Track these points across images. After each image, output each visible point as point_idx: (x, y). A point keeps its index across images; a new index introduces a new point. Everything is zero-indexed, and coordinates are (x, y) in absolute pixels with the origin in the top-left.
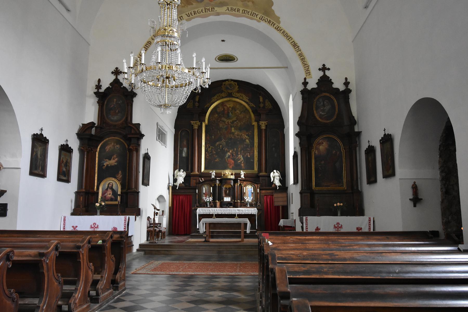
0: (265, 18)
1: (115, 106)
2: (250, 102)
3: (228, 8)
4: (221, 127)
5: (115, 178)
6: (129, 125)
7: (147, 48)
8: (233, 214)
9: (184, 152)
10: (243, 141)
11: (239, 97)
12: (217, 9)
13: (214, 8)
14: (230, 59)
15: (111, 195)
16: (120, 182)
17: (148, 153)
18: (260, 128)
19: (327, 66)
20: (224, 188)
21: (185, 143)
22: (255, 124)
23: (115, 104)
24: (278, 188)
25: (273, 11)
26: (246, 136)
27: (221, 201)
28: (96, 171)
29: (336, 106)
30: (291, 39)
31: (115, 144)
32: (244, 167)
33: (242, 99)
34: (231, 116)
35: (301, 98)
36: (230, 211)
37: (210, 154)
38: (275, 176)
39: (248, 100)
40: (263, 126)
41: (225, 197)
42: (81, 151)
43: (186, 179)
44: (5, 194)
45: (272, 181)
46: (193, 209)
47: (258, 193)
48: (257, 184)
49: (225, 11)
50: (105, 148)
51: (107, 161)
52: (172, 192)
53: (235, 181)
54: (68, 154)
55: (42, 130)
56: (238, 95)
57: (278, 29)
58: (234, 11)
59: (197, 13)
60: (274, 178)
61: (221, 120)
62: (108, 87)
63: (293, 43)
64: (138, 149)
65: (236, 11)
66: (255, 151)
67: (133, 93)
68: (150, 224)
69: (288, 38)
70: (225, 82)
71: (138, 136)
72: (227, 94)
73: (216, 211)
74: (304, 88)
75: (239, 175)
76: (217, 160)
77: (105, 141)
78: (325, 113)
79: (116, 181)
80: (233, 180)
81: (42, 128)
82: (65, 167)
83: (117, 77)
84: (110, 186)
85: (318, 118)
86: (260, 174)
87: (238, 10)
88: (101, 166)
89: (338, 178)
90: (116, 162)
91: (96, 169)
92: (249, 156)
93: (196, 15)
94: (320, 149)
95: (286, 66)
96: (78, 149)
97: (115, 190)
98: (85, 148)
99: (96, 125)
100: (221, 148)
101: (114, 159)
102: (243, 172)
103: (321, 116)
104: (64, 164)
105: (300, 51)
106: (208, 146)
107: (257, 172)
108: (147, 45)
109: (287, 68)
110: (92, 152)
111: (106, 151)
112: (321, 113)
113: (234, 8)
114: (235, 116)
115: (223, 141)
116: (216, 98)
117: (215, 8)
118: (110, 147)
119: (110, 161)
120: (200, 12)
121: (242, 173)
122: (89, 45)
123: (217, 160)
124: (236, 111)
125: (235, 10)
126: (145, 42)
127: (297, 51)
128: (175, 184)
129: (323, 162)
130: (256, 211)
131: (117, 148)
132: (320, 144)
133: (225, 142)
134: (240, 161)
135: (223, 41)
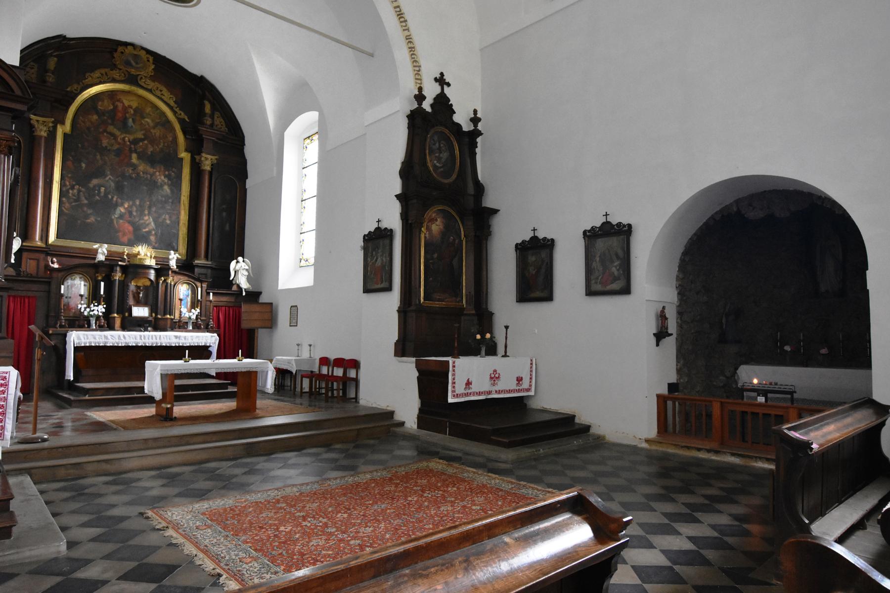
2: (178, 108)
4: (106, 147)
8: (164, 345)
18: (200, 167)
20: (132, 286)
22: (185, 155)
24: (244, 294)
26: (165, 178)
29: (457, 156)
32: (156, 243)
33: (159, 95)
36: (156, 339)
37: (73, 204)
38: (238, 271)
39: (174, 102)
40: (208, 165)
45: (231, 279)
47: (198, 301)
48: (201, 282)
56: (151, 85)
61: (105, 131)
66: (183, 212)
72: (124, 74)
73: (122, 338)
74: (418, 106)
76: (92, 219)
85: (429, 164)
89: (455, 287)
92: (168, 222)
95: (371, 52)
100: (102, 194)
102: (175, 254)
105: (408, 30)
106: (68, 183)
112: (435, 162)
114: (141, 130)
115: (107, 178)
116: (98, 78)
123: (92, 219)
124: (145, 118)
129: (435, 256)
130: (216, 340)
132: (433, 220)
133: (112, 181)
134: (147, 230)
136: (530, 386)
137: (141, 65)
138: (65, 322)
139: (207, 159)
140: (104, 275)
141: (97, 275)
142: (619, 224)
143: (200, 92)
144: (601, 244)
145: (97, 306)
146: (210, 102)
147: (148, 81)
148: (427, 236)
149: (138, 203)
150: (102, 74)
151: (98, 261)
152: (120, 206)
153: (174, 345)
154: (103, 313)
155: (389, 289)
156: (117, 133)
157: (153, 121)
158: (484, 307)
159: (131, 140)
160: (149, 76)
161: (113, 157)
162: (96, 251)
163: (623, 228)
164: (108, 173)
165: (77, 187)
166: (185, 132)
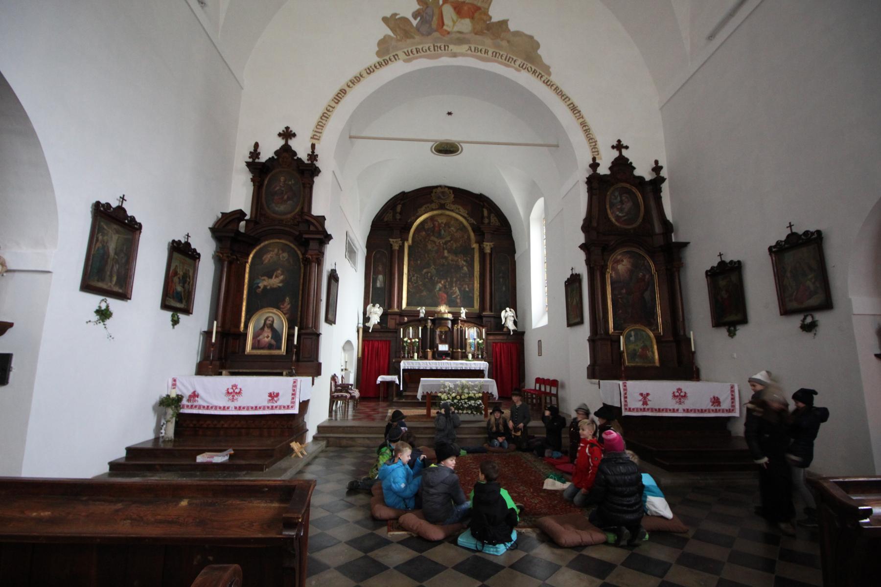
0: (527, 67)
3: (470, 47)
5: (278, 308)
6: (307, 218)
7: (339, 99)
9: (378, 281)
10: (459, 268)
12: (453, 48)
13: (448, 46)
14: (452, 149)
15: (270, 338)
16: (287, 315)
17: (335, 270)
19: (624, 143)
20: (438, 332)
21: (380, 268)
22: (475, 246)
24: (512, 333)
25: (540, 57)
27: (434, 349)
28: (245, 296)
29: (640, 204)
30: (568, 99)
31: (280, 252)
35: (587, 190)
38: (507, 317)
41: (440, 344)
42: (218, 259)
43: (383, 317)
44: (10, 331)
45: (503, 323)
46: (394, 361)
49: (467, 51)
51: (264, 280)
52: (363, 337)
53: (455, 321)
54: (188, 260)
55: (123, 199)
56: (453, 207)
57: (549, 83)
58: (479, 52)
59: (421, 50)
60: (506, 319)
62: (271, 157)
63: (572, 105)
64: (320, 260)
65: (483, 52)
66: (476, 282)
67: (314, 167)
68: (336, 386)
69: (563, 98)
71: (321, 237)
73: (428, 364)
75: (459, 314)
77: (262, 244)
78: (624, 214)
79: (278, 313)
80: (451, 320)
81: (124, 196)
82: (181, 284)
83: (287, 142)
84: (268, 322)
85: (613, 220)
86: (484, 313)
87: (486, 52)
88: (254, 287)
90: (282, 281)
91: (245, 292)
92: (467, 289)
93: (419, 54)
94: (619, 270)
96: (212, 256)
97: (278, 330)
98: (225, 255)
99: (247, 217)
100: (429, 278)
101: (276, 277)
103: (618, 218)
104: (179, 278)
105: (582, 117)
106: (411, 274)
107: (478, 312)
108: (339, 95)
109: (557, 146)
112: (618, 213)
113: (480, 48)
115: (432, 268)
117: (450, 46)
118: (271, 257)
119: (270, 280)
120: (426, 50)
121: (463, 312)
122: (242, 88)
123: (424, 293)
125: (481, 50)
126: (336, 90)
127: (578, 117)
128: (367, 324)
129: (624, 291)
132: (618, 262)
133: (435, 269)
134: (455, 296)
135: (450, 114)
136: (733, 406)
139: (487, 245)
142: (806, 233)
143: (482, 204)
144: (789, 258)
146: (487, 208)
148: (613, 275)
149: (449, 280)
153: (459, 369)
155: (581, 322)
158: (682, 333)
162: (419, 311)
163: (811, 236)
165: (416, 275)
166: (474, 231)
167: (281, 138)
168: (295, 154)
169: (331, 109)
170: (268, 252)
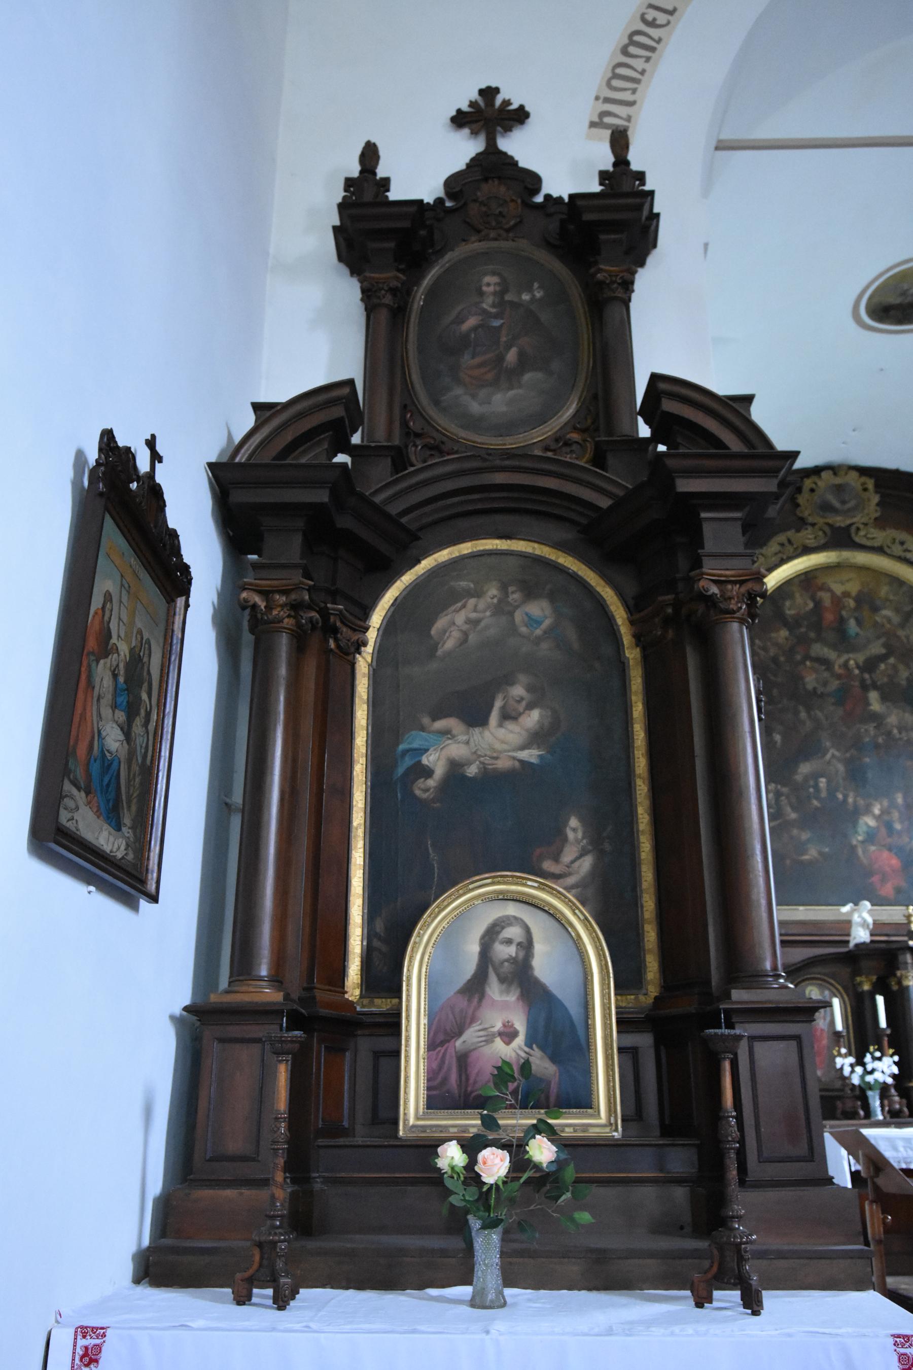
1: (496, 323)
4: (815, 689)
11: (886, 549)
15: (520, 1040)
23: (493, 306)
28: (358, 818)
31: (515, 596)
33: (903, 554)
34: (857, 634)
50: (432, 622)
51: (446, 733)
56: (880, 536)
61: (807, 657)
70: (814, 478)
72: (824, 532)
76: (812, 853)
77: (426, 564)
82: (121, 716)
84: (504, 951)
88: (400, 771)
90: (535, 738)
100: (824, 794)
101: (507, 716)
110: (332, 644)
111: (439, 653)
114: (878, 638)
115: (828, 756)
116: (776, 554)
118: (468, 621)
123: (812, 853)
131: (533, 622)
133: (839, 760)
137: (852, 504)
138: (900, 1103)
140: (874, 978)
141: (858, 979)
145: (880, 1059)
147: (872, 530)
149: (900, 799)
150: (782, 545)
151: (857, 945)
152: (864, 815)
154: (894, 1076)
156: (829, 653)
157: (897, 610)
159: (861, 664)
160: (872, 521)
161: (832, 708)
162: (846, 925)
164: (828, 744)
167: (466, 131)
168: (533, 181)
169: (662, 18)
170: (455, 597)
